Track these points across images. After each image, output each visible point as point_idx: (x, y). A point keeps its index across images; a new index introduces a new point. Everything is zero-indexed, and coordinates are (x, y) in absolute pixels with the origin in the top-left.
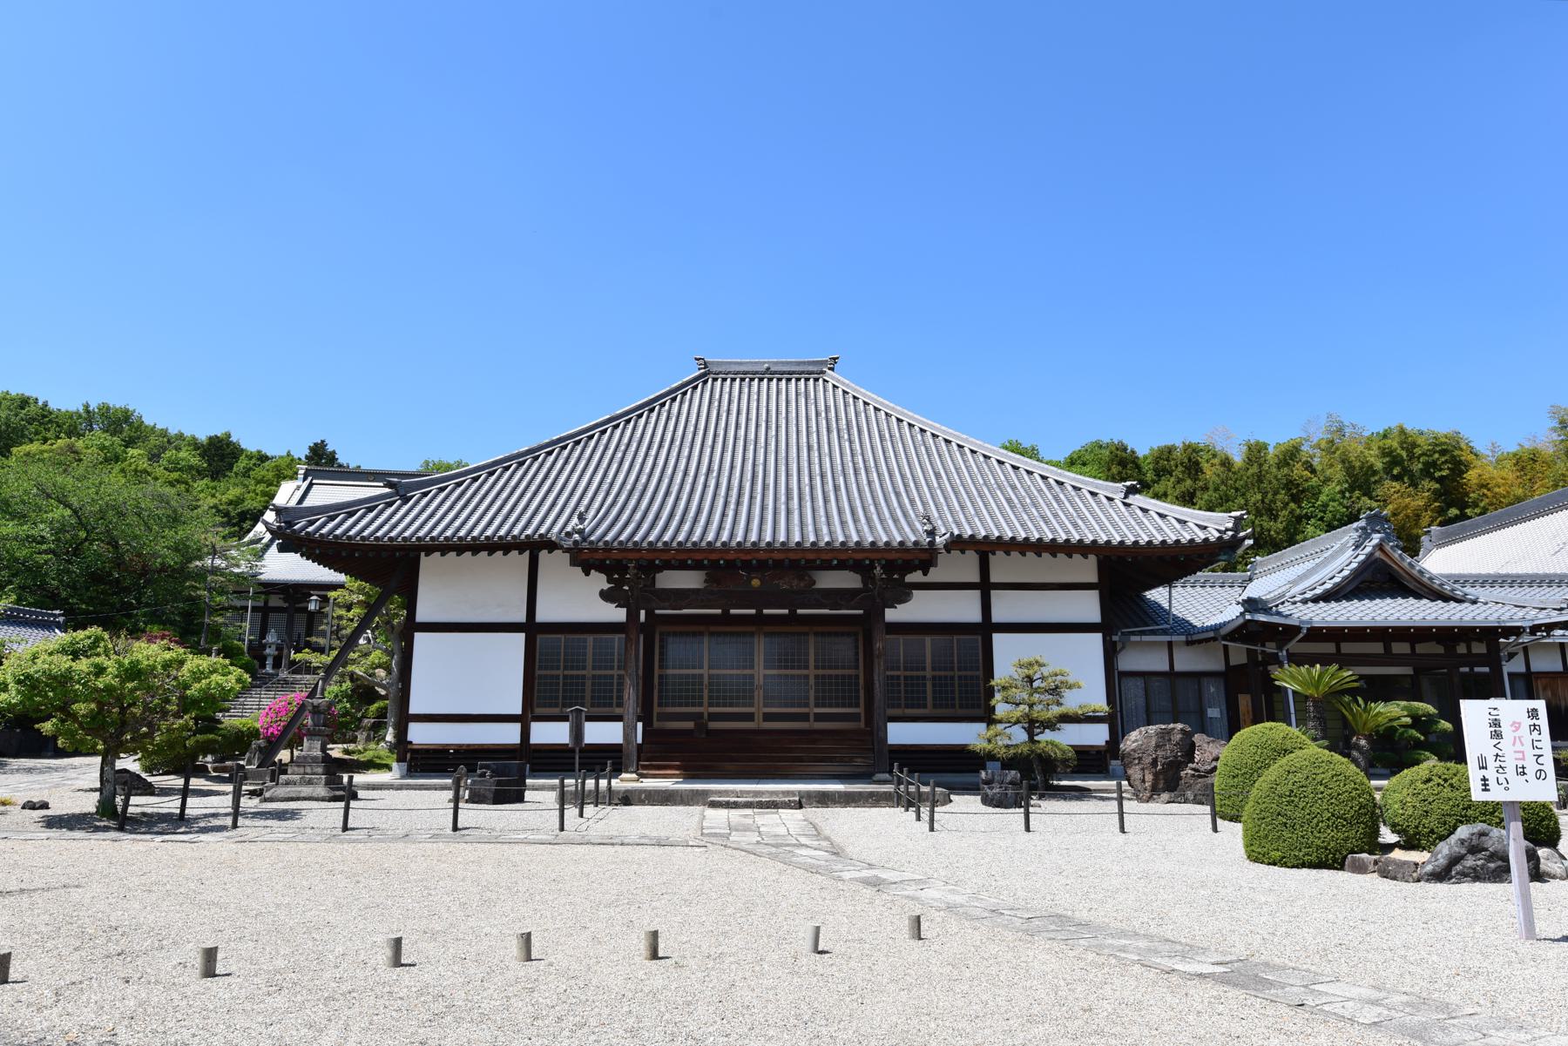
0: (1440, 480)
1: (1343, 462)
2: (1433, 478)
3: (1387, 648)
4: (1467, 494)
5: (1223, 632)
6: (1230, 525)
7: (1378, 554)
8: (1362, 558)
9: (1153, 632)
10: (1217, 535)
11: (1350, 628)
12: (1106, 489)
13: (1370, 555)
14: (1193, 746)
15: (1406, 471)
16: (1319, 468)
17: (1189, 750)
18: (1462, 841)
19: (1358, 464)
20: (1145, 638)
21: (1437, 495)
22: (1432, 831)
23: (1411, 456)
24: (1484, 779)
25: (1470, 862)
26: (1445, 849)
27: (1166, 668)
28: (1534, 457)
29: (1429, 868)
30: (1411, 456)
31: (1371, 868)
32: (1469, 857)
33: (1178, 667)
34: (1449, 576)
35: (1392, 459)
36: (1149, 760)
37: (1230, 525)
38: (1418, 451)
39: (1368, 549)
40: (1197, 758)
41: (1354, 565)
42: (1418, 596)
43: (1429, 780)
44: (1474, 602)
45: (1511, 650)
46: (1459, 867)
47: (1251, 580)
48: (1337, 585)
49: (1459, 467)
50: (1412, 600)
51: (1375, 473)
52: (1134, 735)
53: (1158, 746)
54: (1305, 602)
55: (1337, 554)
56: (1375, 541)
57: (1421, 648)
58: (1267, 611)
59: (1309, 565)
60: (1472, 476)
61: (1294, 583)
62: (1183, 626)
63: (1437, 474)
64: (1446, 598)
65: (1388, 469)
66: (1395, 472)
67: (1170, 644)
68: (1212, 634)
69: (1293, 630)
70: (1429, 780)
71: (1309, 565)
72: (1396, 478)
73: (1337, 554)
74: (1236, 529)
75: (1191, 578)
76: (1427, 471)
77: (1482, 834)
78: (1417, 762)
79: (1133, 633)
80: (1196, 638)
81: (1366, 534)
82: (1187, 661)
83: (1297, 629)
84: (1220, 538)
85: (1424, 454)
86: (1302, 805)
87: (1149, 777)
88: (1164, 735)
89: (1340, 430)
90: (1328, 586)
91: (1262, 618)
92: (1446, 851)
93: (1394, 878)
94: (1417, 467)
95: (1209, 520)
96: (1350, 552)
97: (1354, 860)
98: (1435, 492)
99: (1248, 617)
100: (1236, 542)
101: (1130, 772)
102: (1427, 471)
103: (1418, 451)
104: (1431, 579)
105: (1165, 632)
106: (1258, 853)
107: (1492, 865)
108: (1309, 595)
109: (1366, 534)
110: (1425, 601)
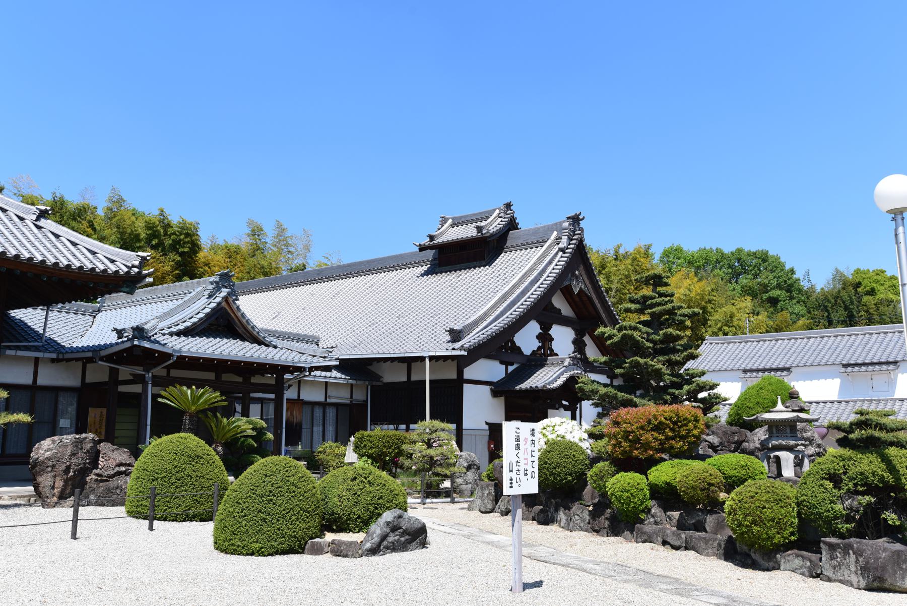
0: (182, 254)
1: (118, 227)
2: (178, 253)
3: (218, 377)
4: (196, 268)
5: (103, 353)
6: (137, 263)
7: (224, 304)
8: (213, 305)
9: (27, 348)
10: (126, 270)
11: (245, 362)
12: (17, 207)
13: (219, 304)
14: (98, 452)
15: (160, 244)
16: (98, 228)
17: (94, 456)
18: (388, 523)
19: (129, 231)
20: (20, 353)
21: (178, 265)
22: (359, 517)
23: (166, 234)
24: (511, 480)
25: (391, 538)
26: (377, 528)
27: (29, 381)
28: (237, 251)
29: (368, 545)
30: (166, 234)
31: (326, 550)
32: (391, 534)
33: (41, 382)
34: (266, 331)
35: (154, 234)
36: (64, 467)
37: (137, 263)
38: (170, 231)
39: (218, 300)
40: (101, 464)
41: (207, 310)
42: (243, 339)
43: (354, 479)
44: (275, 347)
45: (290, 383)
46: (385, 543)
47: (99, 311)
48: (194, 324)
49: (195, 247)
50: (239, 342)
51: (139, 240)
52: (46, 443)
53: (73, 454)
54: (171, 334)
55: (195, 300)
56: (223, 294)
57: (226, 377)
58: (148, 339)
59: (171, 305)
60: (201, 255)
61: (161, 318)
62: (52, 345)
63: (180, 250)
64: (260, 342)
65: (149, 240)
66: (154, 243)
67: (37, 360)
68: (90, 354)
69: (166, 356)
70: (354, 479)
71: (171, 305)
72: (154, 248)
73: (195, 300)
74: (140, 267)
75: (67, 305)
76: (174, 247)
77: (400, 517)
78: (252, 463)
79: (9, 348)
80: (63, 356)
81: (218, 287)
82: (49, 377)
83: (168, 356)
84: (128, 273)
85: (174, 234)
86: (279, 502)
87: (59, 483)
88: (78, 443)
89: (120, 201)
90: (188, 324)
91: (147, 345)
92: (378, 532)
93: (346, 556)
94: (168, 242)
95: (117, 255)
96: (204, 300)
97: (313, 544)
98: (177, 263)
99: (136, 343)
100: (140, 277)
101: (40, 479)
102: (174, 247)
103: (170, 231)
104: (253, 327)
105: (37, 349)
106: (227, 545)
107: (403, 539)
108: (174, 329)
109: (218, 287)
110: (247, 343)
